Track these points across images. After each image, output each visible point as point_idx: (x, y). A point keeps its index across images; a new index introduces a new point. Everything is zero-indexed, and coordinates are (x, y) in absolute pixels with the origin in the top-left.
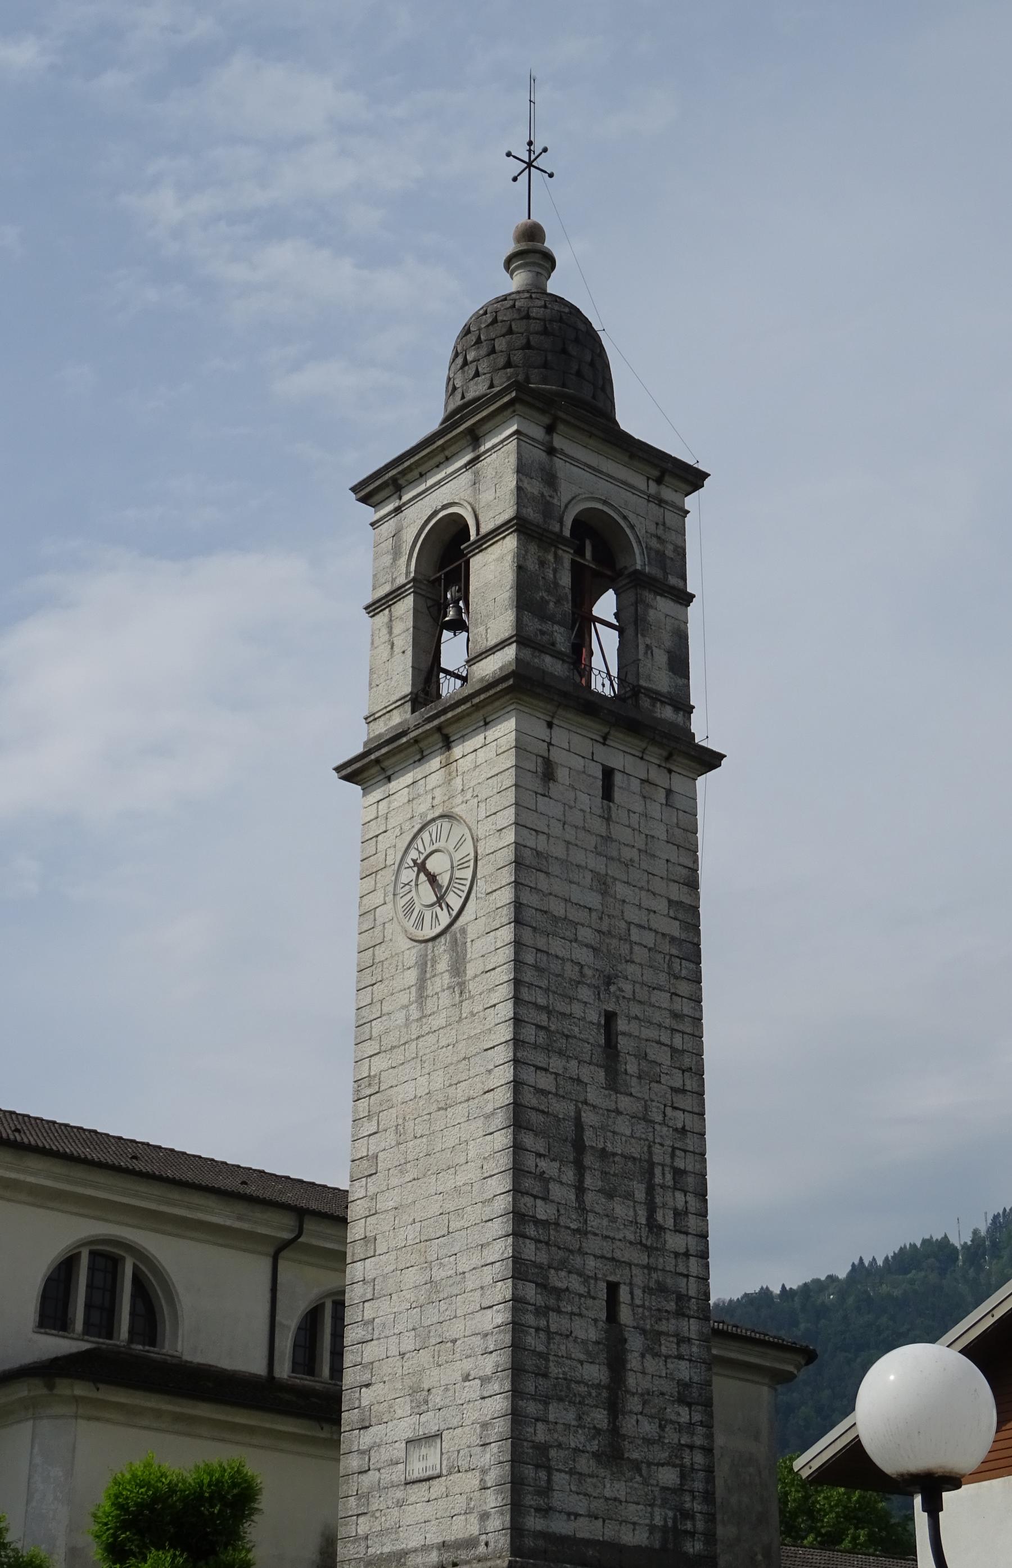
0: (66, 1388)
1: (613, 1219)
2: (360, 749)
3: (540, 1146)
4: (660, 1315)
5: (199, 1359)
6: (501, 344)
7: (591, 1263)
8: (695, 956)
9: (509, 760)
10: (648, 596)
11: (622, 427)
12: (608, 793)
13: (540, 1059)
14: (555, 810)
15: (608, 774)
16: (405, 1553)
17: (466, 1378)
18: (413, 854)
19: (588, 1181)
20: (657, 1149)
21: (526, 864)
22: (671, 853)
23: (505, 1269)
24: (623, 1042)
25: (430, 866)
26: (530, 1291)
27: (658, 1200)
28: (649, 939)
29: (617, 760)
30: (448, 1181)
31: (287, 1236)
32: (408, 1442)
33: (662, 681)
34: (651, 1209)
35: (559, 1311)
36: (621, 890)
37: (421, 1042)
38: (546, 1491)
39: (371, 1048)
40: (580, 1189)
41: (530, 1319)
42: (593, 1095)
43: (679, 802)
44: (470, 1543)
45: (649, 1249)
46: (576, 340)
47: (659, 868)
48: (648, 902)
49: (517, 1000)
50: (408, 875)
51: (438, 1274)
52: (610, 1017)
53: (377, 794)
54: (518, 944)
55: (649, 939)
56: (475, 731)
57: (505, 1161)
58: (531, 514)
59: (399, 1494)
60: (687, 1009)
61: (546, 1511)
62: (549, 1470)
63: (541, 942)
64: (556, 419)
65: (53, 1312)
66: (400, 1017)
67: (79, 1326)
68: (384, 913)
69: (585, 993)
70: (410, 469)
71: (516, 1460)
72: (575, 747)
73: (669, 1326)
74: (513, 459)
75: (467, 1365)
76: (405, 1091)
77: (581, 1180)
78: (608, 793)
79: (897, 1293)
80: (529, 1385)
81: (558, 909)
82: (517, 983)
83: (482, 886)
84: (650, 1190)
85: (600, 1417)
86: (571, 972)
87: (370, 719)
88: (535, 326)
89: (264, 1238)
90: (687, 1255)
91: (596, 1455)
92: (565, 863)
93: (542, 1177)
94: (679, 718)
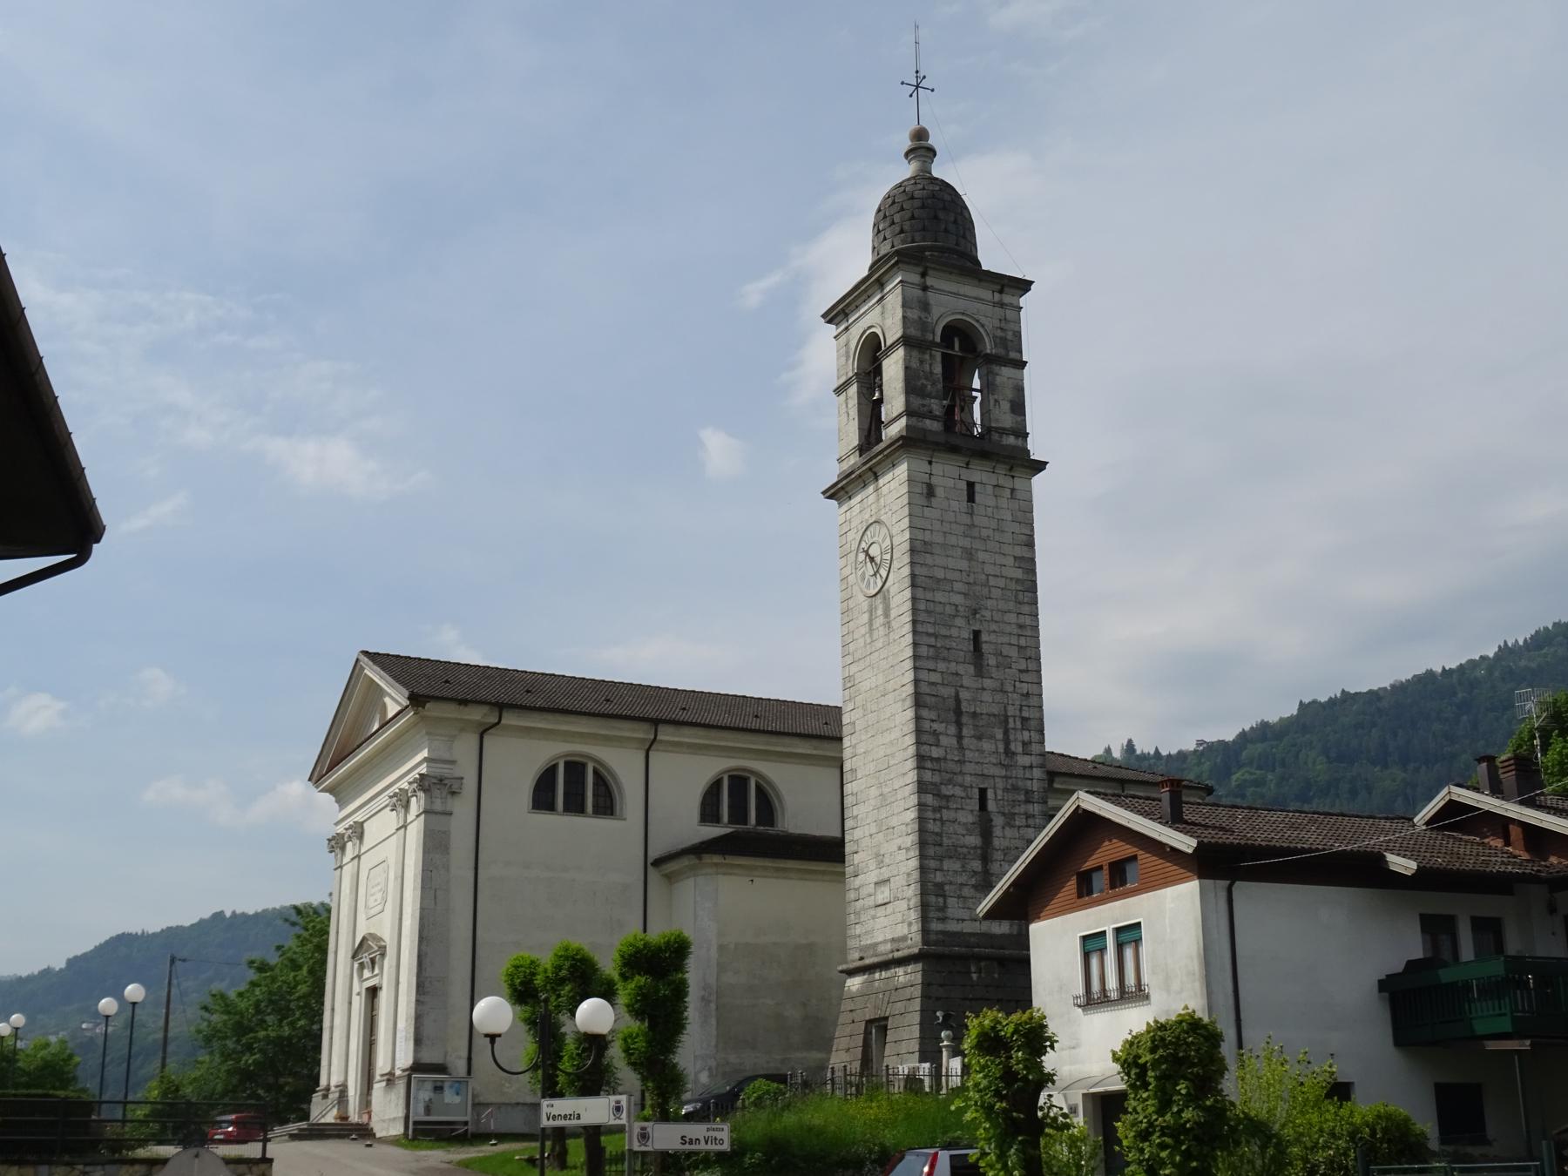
0: (707, 859)
1: (981, 751)
2: (835, 480)
3: (933, 715)
4: (1014, 803)
5: (798, 831)
6: (897, 218)
7: (968, 779)
8: (1033, 588)
9: (905, 489)
10: (996, 368)
11: (187, 924)
12: (971, 498)
13: (931, 665)
14: (935, 514)
15: (971, 485)
16: (876, 944)
18: (863, 545)
19: (965, 732)
20: (1010, 708)
21: (917, 550)
22: (1016, 528)
23: (912, 788)
24: (985, 647)
25: (871, 552)
26: (929, 799)
27: (1012, 737)
28: (1001, 583)
29: (975, 476)
30: (888, 737)
33: (1006, 419)
34: (1007, 742)
35: (948, 808)
36: (981, 556)
38: (944, 908)
39: (849, 659)
40: (960, 737)
41: (930, 814)
42: (966, 682)
43: (1019, 495)
44: (904, 938)
45: (1006, 767)
46: (944, 208)
47: (1008, 538)
48: (1000, 560)
49: (915, 632)
50: (862, 556)
51: (886, 790)
52: (977, 634)
53: (845, 507)
54: (914, 599)
55: (1001, 583)
57: (912, 726)
58: (913, 332)
59: (872, 912)
60: (1028, 621)
61: (943, 920)
62: (945, 897)
63: (929, 596)
64: (926, 268)
65: (709, 812)
66: (861, 641)
67: (725, 818)
68: (852, 579)
69: (959, 622)
71: (924, 893)
72: (948, 474)
73: (1022, 809)
74: (900, 298)
75: (899, 841)
76: (865, 686)
77: (960, 730)
78: (971, 498)
79: (1533, 665)
80: (931, 851)
81: (940, 574)
82: (914, 622)
83: (896, 565)
84: (1006, 732)
85: (976, 865)
86: (949, 610)
87: (840, 460)
88: (917, 203)
90: (1031, 767)
91: (973, 886)
92: (944, 546)
93: (935, 734)
94: (1020, 442)
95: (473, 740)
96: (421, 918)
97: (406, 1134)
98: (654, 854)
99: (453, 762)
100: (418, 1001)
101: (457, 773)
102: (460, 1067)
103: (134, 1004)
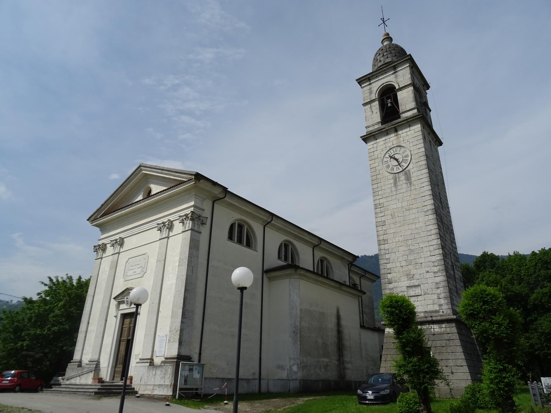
2: (365, 134)
17: (428, 272)
31: (317, 244)
32: (408, 287)
37: (397, 196)
56: (406, 128)
70: (374, 75)
89: (311, 243)
95: (210, 203)
96: (186, 280)
97: (174, 396)
98: (265, 268)
99: (203, 210)
100: (182, 322)
101: (204, 215)
102: (195, 357)
103: (242, 289)
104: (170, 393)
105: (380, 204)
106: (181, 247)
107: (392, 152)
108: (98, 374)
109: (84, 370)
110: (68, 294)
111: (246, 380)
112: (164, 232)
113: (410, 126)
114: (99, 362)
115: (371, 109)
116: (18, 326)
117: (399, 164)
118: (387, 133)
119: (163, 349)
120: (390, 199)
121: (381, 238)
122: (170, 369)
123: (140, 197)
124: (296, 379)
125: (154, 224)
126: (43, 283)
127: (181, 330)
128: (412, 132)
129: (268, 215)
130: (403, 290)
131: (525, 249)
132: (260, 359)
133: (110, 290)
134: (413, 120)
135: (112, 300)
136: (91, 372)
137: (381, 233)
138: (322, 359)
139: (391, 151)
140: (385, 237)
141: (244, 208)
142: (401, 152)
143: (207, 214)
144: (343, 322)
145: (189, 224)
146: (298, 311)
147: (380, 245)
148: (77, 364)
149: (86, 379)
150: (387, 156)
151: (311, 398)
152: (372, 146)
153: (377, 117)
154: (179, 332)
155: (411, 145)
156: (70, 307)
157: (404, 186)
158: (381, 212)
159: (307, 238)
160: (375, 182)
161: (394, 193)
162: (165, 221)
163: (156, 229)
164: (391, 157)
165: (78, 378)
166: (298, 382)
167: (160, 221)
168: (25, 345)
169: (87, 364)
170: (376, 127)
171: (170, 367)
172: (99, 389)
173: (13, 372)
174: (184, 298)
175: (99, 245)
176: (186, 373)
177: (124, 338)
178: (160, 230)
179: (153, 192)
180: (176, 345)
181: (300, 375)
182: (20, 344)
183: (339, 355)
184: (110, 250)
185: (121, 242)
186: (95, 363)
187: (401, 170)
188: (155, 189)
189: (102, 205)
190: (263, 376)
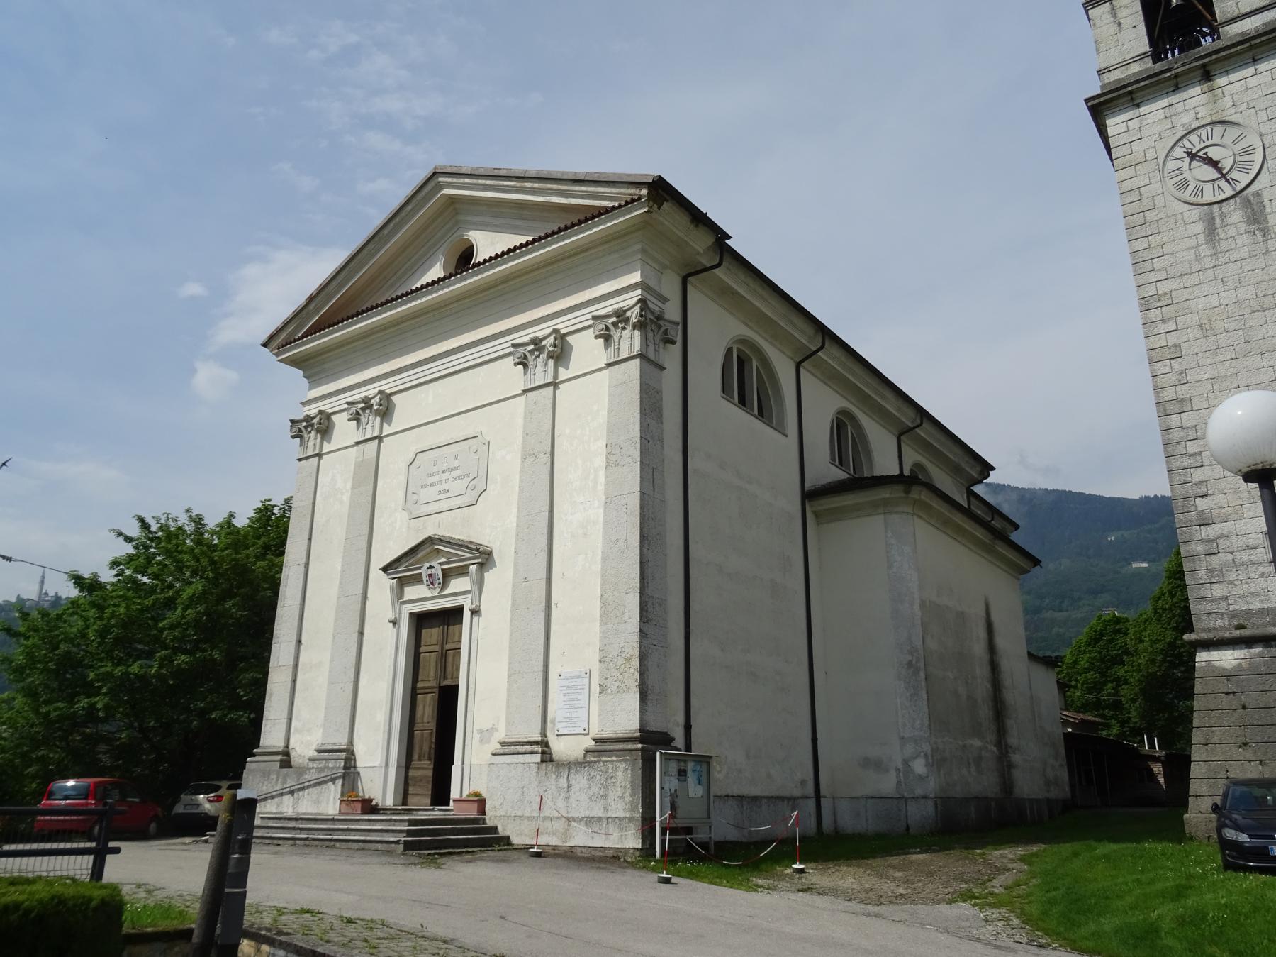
37: (1218, 270)
56: (1244, 66)
96: (642, 508)
97: (647, 851)
98: (808, 485)
100: (643, 634)
102: (678, 735)
104: (632, 841)
105: (1159, 297)
106: (610, 411)
107: (1195, 143)
108: (354, 787)
109: (307, 777)
110: (213, 562)
111: (789, 799)
112: (540, 369)
113: (1255, 61)
114: (353, 753)
115: (1115, 16)
116: (68, 652)
117: (1224, 176)
118: (1172, 83)
119: (582, 714)
120: (1194, 279)
121: (1169, 394)
122: (623, 775)
123: (436, 272)
124: (925, 797)
125: (504, 345)
126: (120, 534)
127: (643, 657)
128: (1266, 77)
129: (810, 330)
130: (1252, 543)
131: (1136, 495)
132: (814, 740)
133: (363, 544)
134: (1268, 42)
135: (376, 574)
136: (333, 780)
137: (1165, 380)
138: (969, 742)
139: (1193, 137)
140: (1183, 391)
141: (757, 304)
142: (1228, 140)
143: (672, 312)
144: (1000, 642)
145: (630, 341)
146: (917, 607)
147: (1164, 414)
148: (279, 757)
149: (317, 802)
150: (1179, 152)
151: (1034, 849)
152: (1123, 127)
153: (1135, 39)
154: (636, 662)
155: (1263, 116)
156: (222, 599)
157: (1244, 239)
158: (1164, 321)
159: (891, 405)
160: (1140, 232)
161: (1208, 262)
162: (539, 334)
163: (510, 360)
164: (1192, 156)
165: (288, 800)
166: (930, 803)
167: (524, 337)
168: (99, 706)
169: (312, 760)
170: (1135, 68)
171: (622, 766)
172: (409, 833)
173: (71, 783)
174: (641, 563)
175: (308, 419)
176: (673, 783)
177: (429, 678)
178: (523, 363)
179: (480, 257)
180: (632, 701)
181: (932, 786)
182: (83, 703)
183: (999, 731)
184: (344, 430)
185: (385, 409)
186: (343, 755)
187: (1229, 192)
188: (486, 243)
189: (311, 299)
190: (824, 790)
